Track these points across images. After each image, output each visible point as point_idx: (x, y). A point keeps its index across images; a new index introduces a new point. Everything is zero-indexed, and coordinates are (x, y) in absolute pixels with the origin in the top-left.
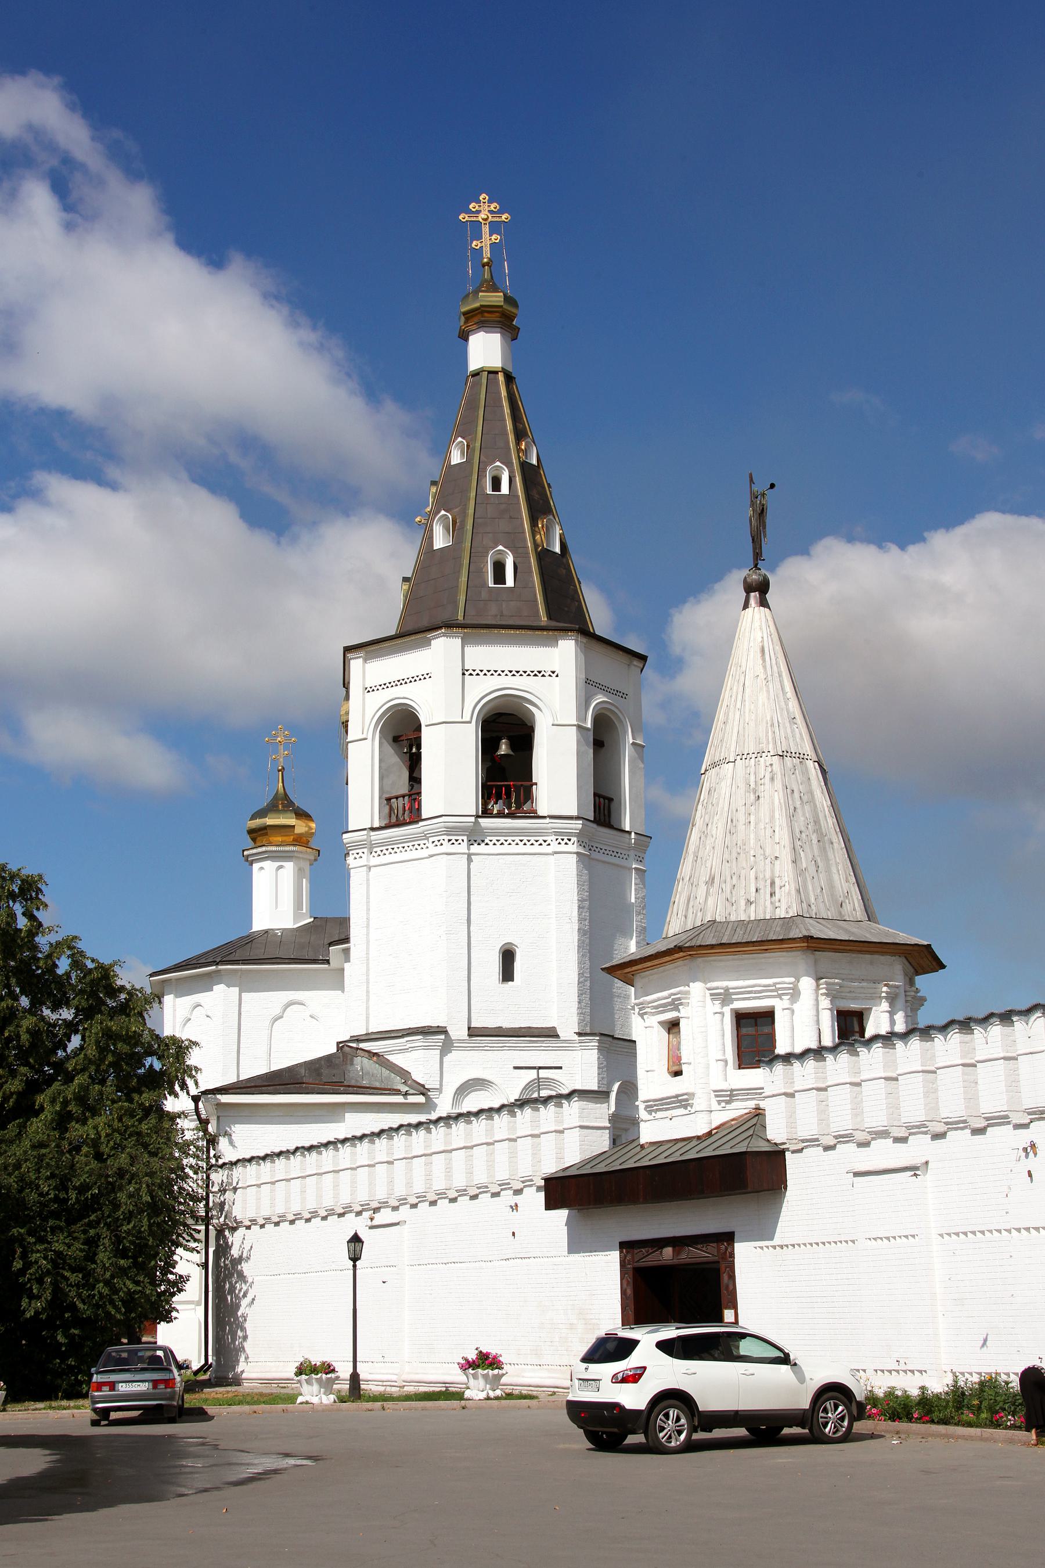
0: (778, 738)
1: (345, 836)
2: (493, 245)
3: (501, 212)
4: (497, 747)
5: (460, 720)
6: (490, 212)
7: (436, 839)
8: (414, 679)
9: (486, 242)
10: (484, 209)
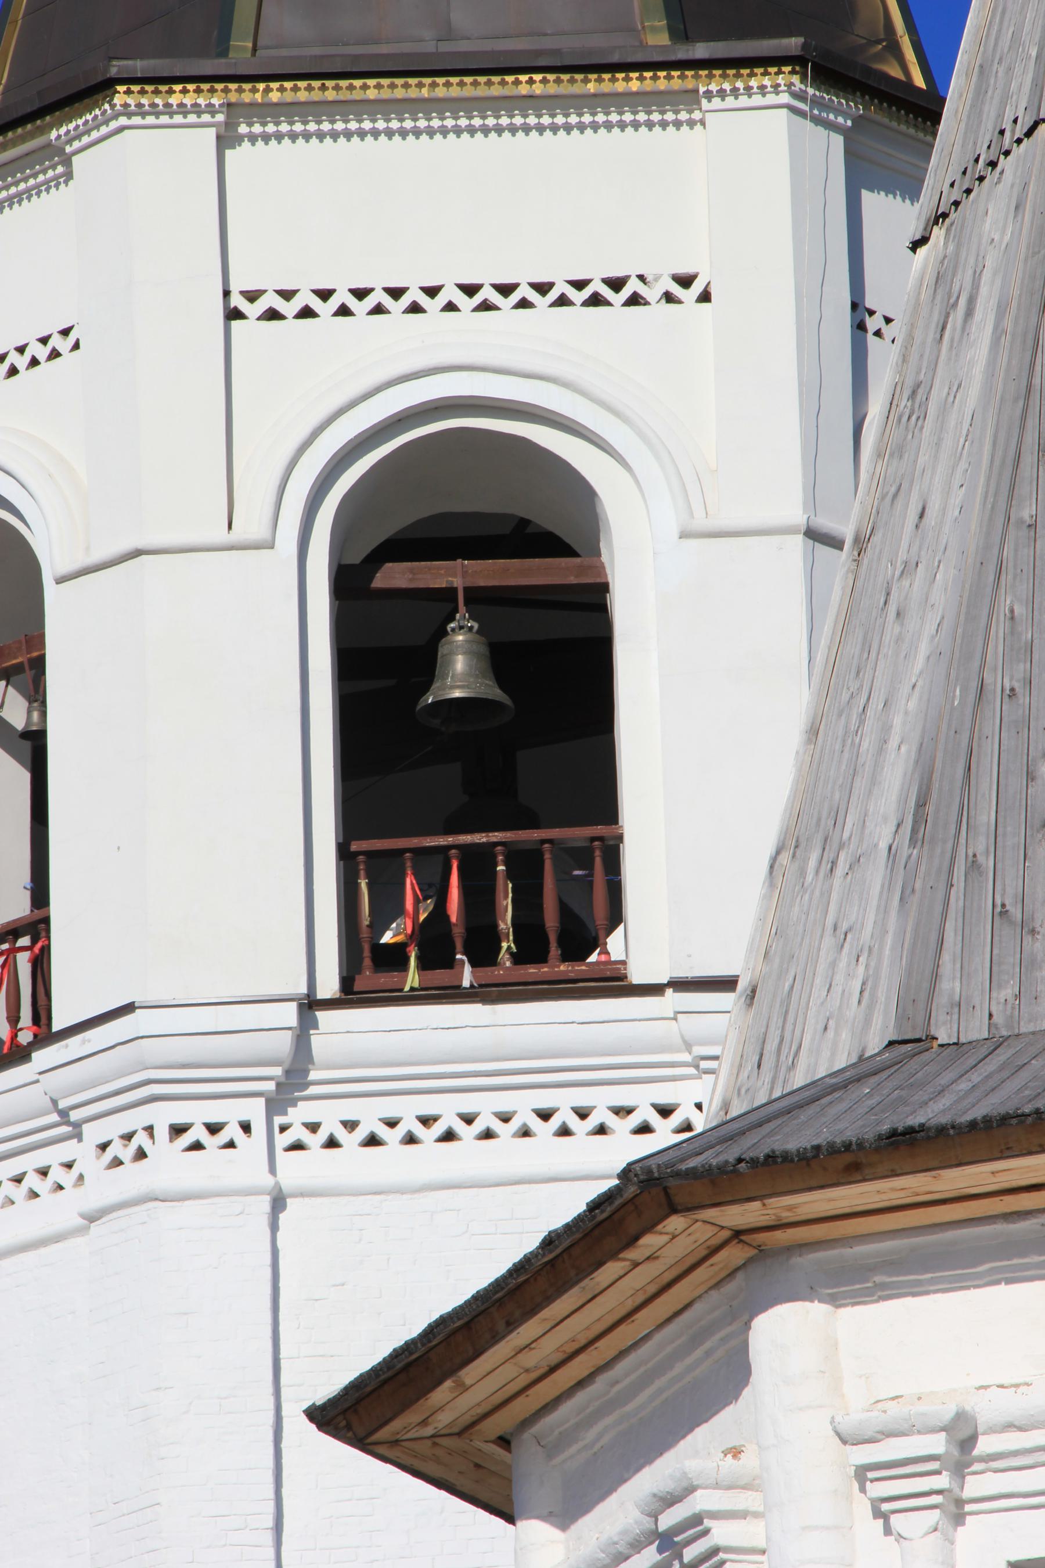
4: (426, 663)
5: (219, 534)
7: (111, 1128)
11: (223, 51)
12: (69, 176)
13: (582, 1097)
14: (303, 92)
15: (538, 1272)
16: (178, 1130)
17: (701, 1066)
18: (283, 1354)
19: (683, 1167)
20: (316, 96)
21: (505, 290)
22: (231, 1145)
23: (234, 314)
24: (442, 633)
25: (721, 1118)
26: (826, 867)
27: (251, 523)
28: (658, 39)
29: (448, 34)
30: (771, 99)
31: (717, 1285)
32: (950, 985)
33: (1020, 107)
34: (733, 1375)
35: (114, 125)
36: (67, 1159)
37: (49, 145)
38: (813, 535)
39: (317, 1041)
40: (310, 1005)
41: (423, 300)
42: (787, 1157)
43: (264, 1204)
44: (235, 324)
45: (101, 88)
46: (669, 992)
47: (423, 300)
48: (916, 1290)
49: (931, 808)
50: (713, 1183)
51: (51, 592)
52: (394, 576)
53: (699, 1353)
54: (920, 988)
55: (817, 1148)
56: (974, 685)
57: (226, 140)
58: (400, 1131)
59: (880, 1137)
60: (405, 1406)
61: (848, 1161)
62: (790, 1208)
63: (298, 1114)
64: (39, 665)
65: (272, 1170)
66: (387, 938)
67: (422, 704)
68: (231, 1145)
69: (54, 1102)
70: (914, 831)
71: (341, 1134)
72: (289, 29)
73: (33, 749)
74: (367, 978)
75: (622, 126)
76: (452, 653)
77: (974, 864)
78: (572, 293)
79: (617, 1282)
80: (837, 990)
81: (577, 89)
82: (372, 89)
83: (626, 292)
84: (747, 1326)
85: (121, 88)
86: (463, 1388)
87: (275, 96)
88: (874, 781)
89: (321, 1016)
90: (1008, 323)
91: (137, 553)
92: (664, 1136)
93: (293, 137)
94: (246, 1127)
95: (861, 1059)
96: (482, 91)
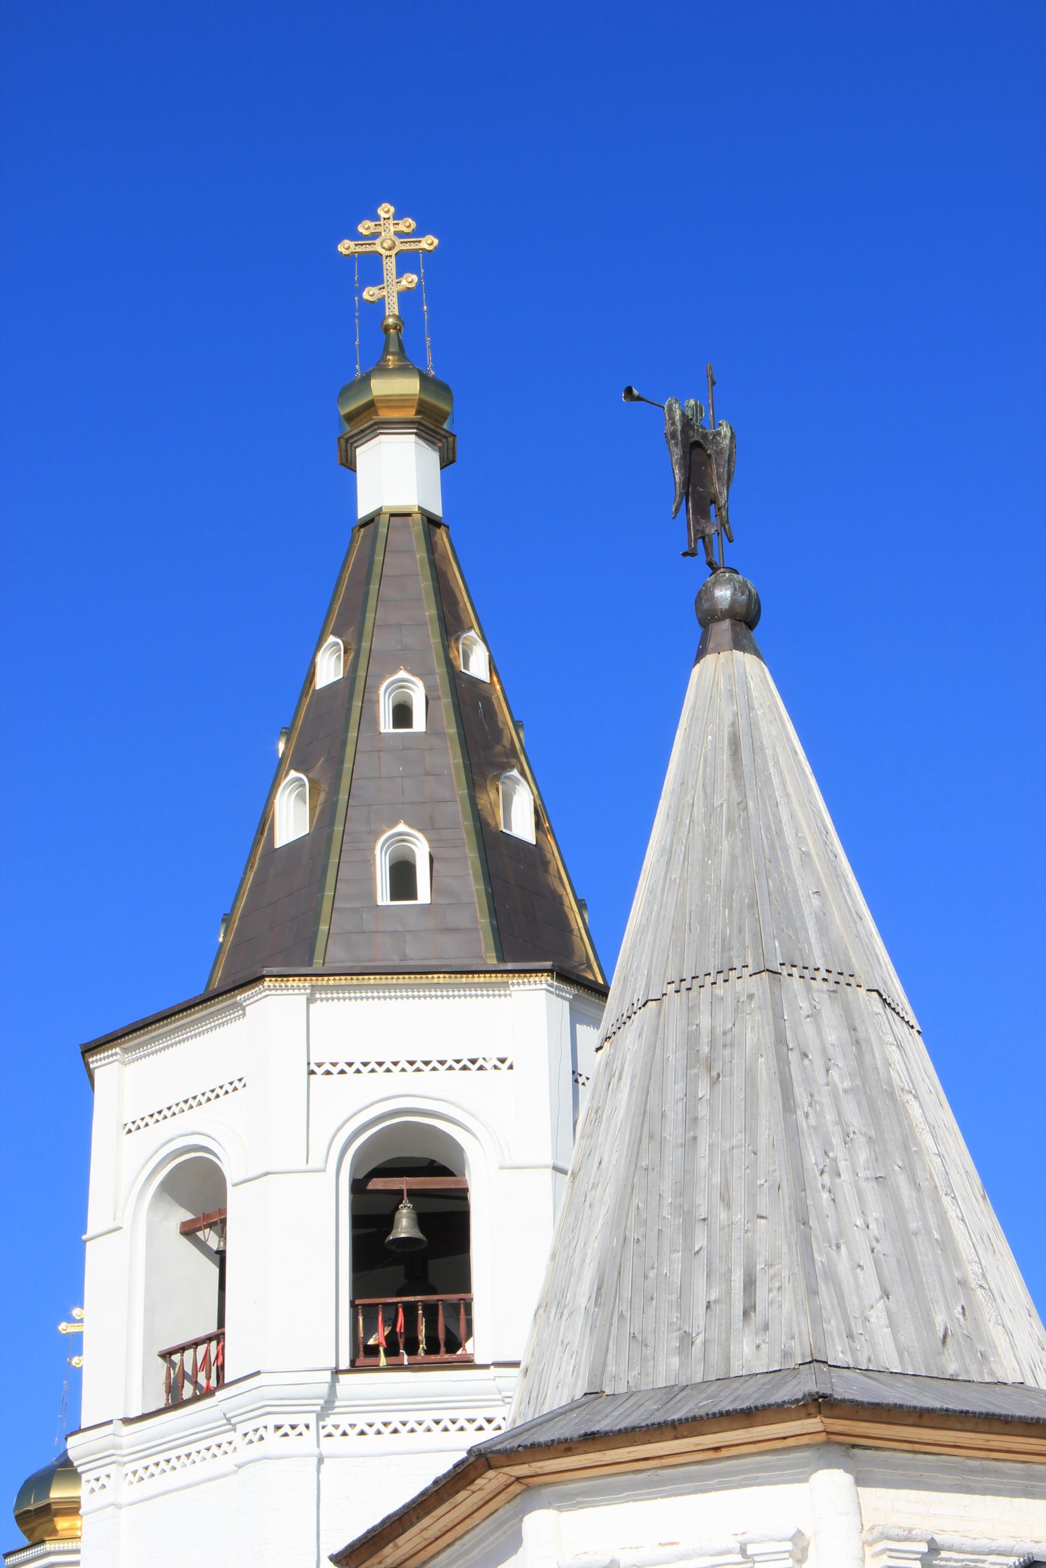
0: (912, 1044)
1: (72, 1441)
2: (405, 296)
3: (419, 233)
4: (388, 1221)
5: (303, 1166)
6: (400, 234)
7: (248, 1427)
8: (215, 1094)
9: (389, 291)
10: (387, 231)
11: (311, 964)
12: (244, 1015)
13: (453, 1414)
14: (343, 981)
15: (431, 1495)
16: (278, 1428)
17: (505, 1400)
18: (321, 1529)
19: (495, 1449)
20: (349, 982)
21: (427, 1063)
22: (301, 1434)
23: (312, 1072)
24: (397, 1209)
25: (512, 1426)
26: (559, 1315)
27: (316, 1161)
28: (492, 961)
29: (404, 958)
30: (539, 986)
31: (509, 1502)
32: (611, 1368)
33: (640, 995)
34: (515, 1541)
35: (264, 994)
36: (229, 1440)
37: (236, 1002)
38: (556, 1169)
39: (339, 1387)
40: (337, 1372)
41: (392, 1067)
42: (539, 1445)
43: (315, 1460)
44: (312, 1076)
45: (257, 980)
46: (492, 1367)
47: (392, 1067)
48: (594, 1504)
49: (603, 1290)
50: (508, 1456)
51: (231, 1191)
52: (377, 1184)
53: (500, 1532)
54: (598, 1370)
55: (553, 1441)
56: (622, 1237)
57: (310, 1000)
58: (374, 1429)
59: (580, 1436)
60: (372, 1554)
61: (566, 1447)
62: (541, 1468)
63: (330, 1421)
64: (224, 1221)
65: (318, 1446)
66: (371, 1342)
67: (387, 1240)
68: (301, 1434)
69: (225, 1415)
70: (596, 1300)
71: (349, 1430)
72: (338, 954)
73: (220, 1259)
74: (362, 1360)
75: (477, 996)
76: (401, 1217)
77: (621, 1315)
78: (455, 1065)
79: (466, 1500)
80: (563, 1370)
81: (458, 981)
82: (372, 980)
83: (477, 1065)
84: (521, 1520)
85: (267, 979)
86: (397, 1547)
87: (331, 983)
88: (579, 1278)
89: (341, 1377)
90: (636, 1083)
91: (268, 1174)
92: (489, 1434)
93: (339, 999)
94: (307, 1427)
95: (572, 1401)
96: (418, 981)
